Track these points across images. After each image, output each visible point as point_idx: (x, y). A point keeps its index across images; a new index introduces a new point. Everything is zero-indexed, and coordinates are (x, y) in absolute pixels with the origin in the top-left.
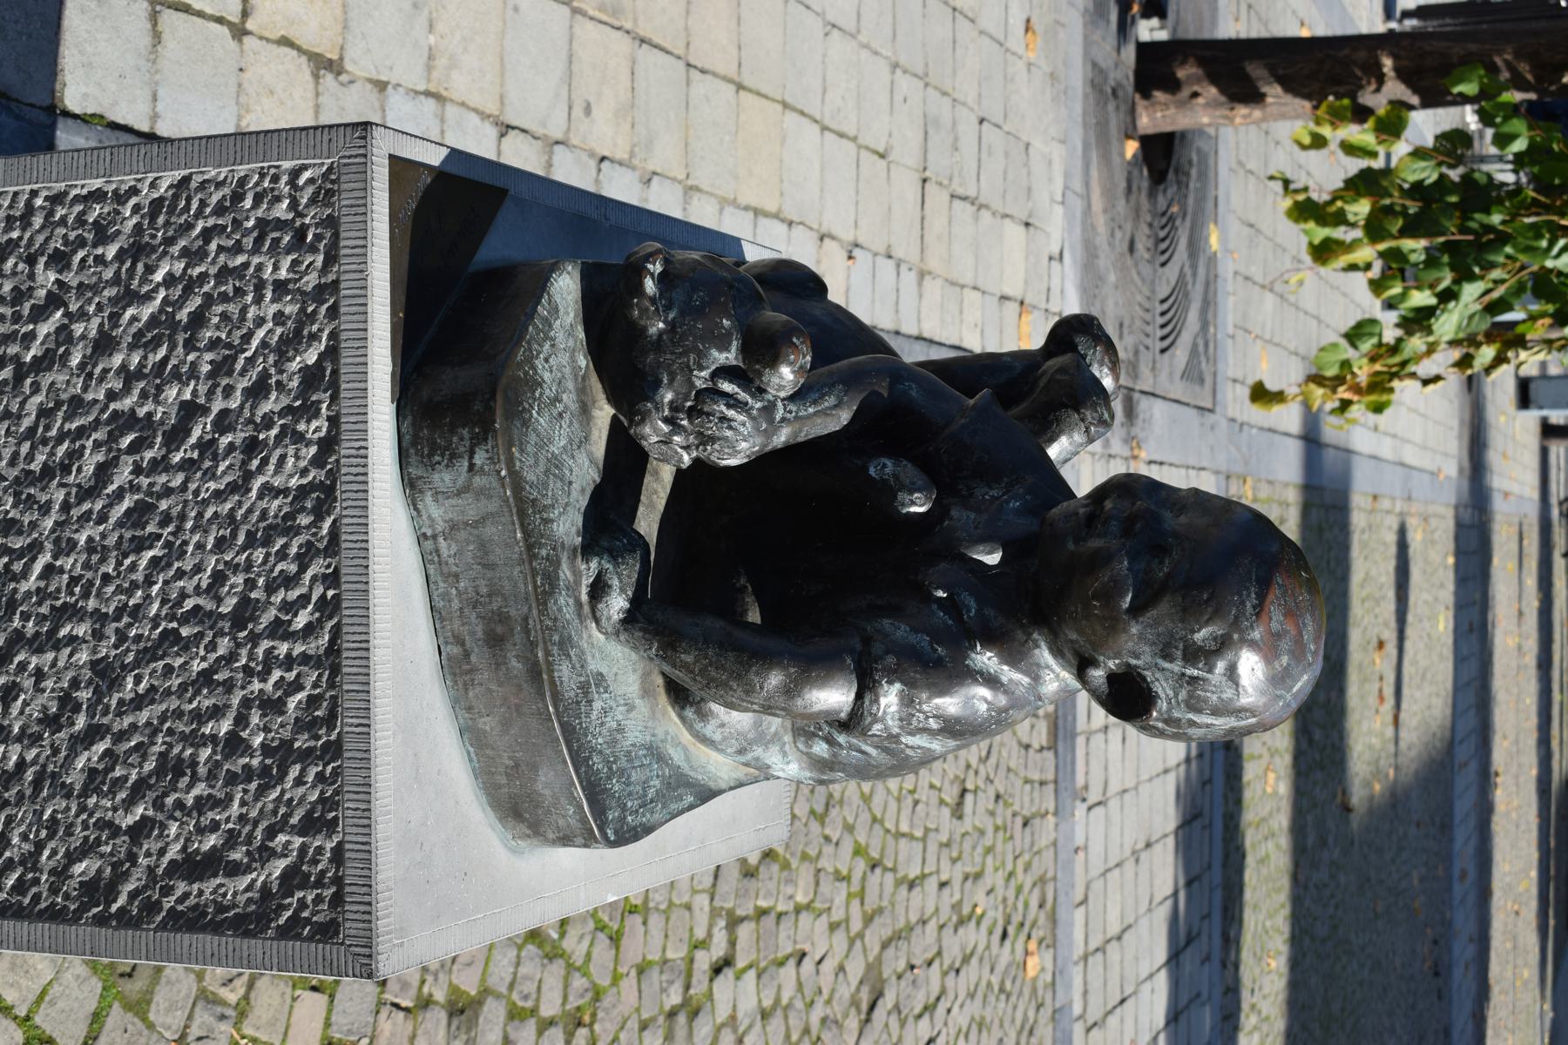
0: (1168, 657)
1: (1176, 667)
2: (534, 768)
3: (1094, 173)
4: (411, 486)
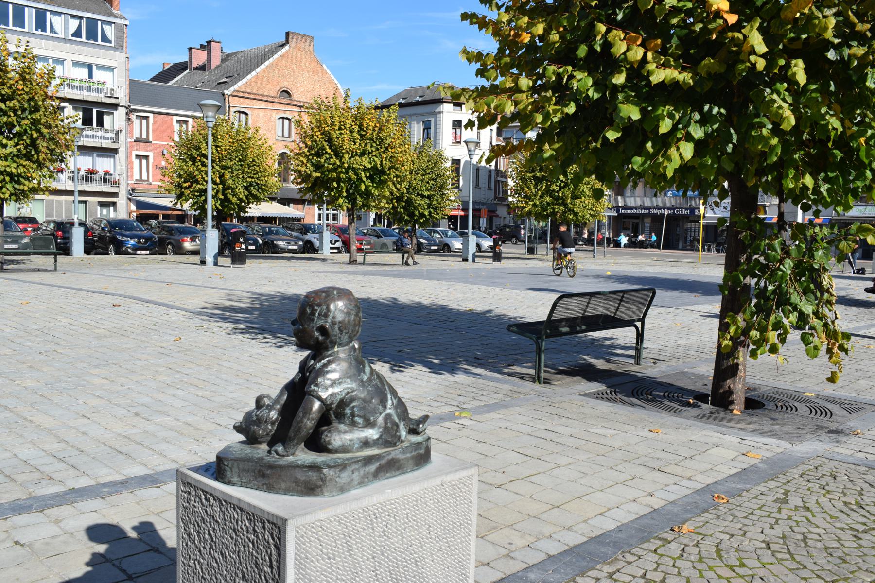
0: (313, 320)
1: (316, 319)
2: (296, 478)
3: (732, 425)
4: (229, 483)
